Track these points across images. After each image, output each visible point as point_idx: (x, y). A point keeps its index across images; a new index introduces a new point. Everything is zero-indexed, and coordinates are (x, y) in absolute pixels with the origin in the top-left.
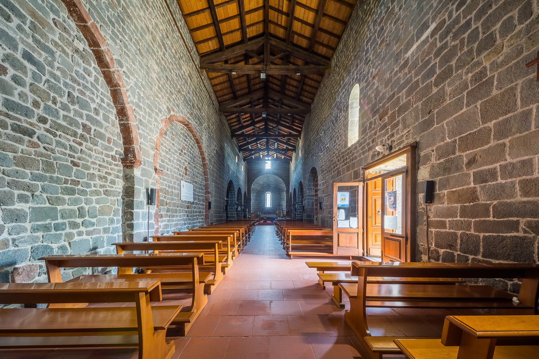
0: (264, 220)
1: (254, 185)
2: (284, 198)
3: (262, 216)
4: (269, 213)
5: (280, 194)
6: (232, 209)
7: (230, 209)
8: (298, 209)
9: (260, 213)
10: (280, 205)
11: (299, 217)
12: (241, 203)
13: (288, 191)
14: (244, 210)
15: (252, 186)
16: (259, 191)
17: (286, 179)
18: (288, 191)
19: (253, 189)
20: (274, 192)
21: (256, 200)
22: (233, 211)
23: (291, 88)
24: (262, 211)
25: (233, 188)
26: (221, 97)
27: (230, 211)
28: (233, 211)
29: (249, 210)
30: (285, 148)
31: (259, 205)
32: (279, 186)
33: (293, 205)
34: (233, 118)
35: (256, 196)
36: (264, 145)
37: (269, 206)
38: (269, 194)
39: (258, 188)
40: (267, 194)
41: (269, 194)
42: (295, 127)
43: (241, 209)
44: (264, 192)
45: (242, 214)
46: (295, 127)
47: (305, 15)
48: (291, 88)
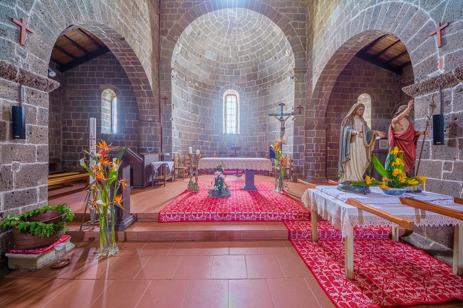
16: (205, 85)
17: (295, 25)
20: (248, 90)
37: (234, 131)
40: (229, 99)
41: (234, 99)
44: (218, 88)
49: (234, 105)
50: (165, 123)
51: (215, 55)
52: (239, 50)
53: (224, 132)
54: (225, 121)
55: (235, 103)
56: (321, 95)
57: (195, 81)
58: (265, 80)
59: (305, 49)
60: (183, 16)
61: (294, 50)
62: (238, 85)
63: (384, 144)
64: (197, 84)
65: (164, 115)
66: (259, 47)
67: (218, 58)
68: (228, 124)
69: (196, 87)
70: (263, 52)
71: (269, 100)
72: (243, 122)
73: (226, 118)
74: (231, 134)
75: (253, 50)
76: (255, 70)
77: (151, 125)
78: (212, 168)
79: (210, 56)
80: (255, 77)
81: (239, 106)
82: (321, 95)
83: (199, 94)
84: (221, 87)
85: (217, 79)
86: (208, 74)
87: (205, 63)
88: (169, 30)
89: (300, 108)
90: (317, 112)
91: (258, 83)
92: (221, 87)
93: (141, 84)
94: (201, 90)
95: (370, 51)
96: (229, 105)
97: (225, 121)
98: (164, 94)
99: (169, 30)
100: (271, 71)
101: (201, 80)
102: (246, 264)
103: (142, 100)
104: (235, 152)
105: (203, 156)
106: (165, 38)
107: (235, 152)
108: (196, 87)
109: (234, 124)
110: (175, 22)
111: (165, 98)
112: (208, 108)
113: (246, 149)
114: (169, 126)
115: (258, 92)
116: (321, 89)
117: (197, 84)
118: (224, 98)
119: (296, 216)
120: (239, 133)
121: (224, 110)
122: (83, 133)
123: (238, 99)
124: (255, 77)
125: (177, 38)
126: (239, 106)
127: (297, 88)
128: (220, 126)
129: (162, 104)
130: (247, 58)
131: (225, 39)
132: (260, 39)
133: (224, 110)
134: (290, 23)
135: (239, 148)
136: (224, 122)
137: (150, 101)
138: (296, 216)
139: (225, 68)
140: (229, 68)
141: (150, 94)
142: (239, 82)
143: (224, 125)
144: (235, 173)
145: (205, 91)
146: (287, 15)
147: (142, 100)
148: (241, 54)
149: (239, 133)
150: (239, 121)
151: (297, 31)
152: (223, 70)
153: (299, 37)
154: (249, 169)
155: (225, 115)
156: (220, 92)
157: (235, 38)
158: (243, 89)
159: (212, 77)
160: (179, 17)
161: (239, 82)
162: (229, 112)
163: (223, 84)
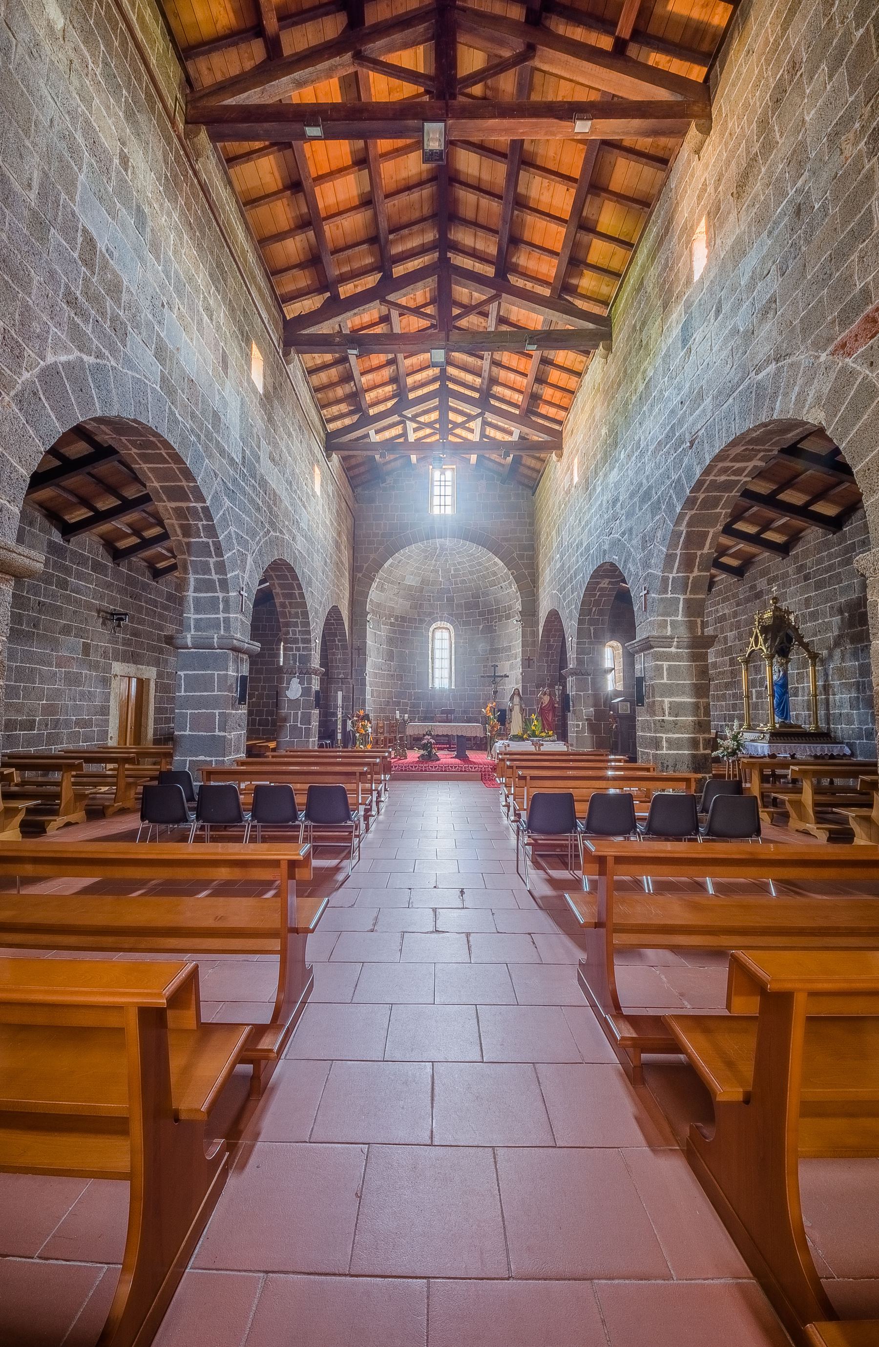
0: (424, 747)
1: (381, 588)
2: (509, 648)
3: (415, 728)
4: (448, 716)
5: (489, 630)
6: (206, 683)
7: (193, 683)
8: (669, 690)
9: (403, 712)
10: (495, 679)
11: (671, 744)
12: (305, 660)
13: (529, 613)
14: (323, 700)
15: (374, 594)
16: (403, 619)
17: (521, 557)
18: (529, 613)
19: (379, 605)
20: (466, 623)
21: (390, 656)
22: (215, 702)
23: (507, 393)
24: (414, 706)
25: (211, 531)
26: (330, 421)
27: (188, 702)
28: (215, 702)
29: (355, 700)
30: (515, 438)
31: (400, 678)
32: (486, 594)
33: (574, 673)
34: (338, 402)
35: (391, 641)
36: (430, 425)
37: (445, 684)
38: (446, 635)
39: (400, 605)
40: (438, 634)
41: (446, 635)
42: (540, 421)
43: (306, 692)
44: (421, 621)
45: (307, 720)
46: (540, 421)
47: (512, 376)
48: (507, 393)
49: (446, 644)
50: (357, 680)
51: (419, 579)
52: (452, 572)
53: (430, 686)
54: (433, 667)
55: (448, 651)
56: (550, 647)
57: (390, 616)
58: (490, 612)
59: (534, 587)
60: (382, 548)
61: (520, 588)
62: (451, 615)
63: (625, 708)
64: (392, 620)
65: (356, 670)
66: (479, 571)
67: (422, 582)
68: (437, 673)
69: (392, 624)
70: (484, 577)
71: (496, 641)
72: (461, 670)
73: (433, 663)
74: (442, 690)
75: (471, 573)
76: (476, 596)
77: (342, 683)
78: (421, 733)
79: (411, 581)
80: (476, 605)
81: (453, 646)
82: (550, 647)
83: (394, 632)
84: (426, 619)
85: (420, 608)
86: (408, 604)
87: (405, 590)
88: (365, 565)
89: (529, 659)
90: (549, 666)
91: (481, 614)
92: (426, 619)
93: (337, 637)
94: (399, 626)
95: (771, 487)
96: (437, 644)
97: (433, 667)
98: (357, 643)
99: (365, 565)
100: (497, 601)
101: (398, 613)
102: (478, 1020)
103: (334, 654)
104: (447, 717)
105: (412, 720)
106: (360, 575)
107: (447, 717)
108: (392, 624)
109: (446, 673)
110: (372, 556)
111: (359, 649)
112: (407, 651)
113: (465, 712)
114: (364, 684)
115: (481, 627)
116: (549, 641)
117: (392, 620)
118: (430, 634)
119: (491, 769)
120: (453, 687)
121: (430, 652)
122: (256, 693)
123: (453, 635)
124: (476, 605)
125: (375, 576)
126: (453, 646)
127: (524, 635)
128: (423, 677)
129: (355, 656)
130: (463, 582)
131: (433, 562)
132: (480, 564)
133: (430, 652)
134: (515, 555)
135: (451, 712)
136: (430, 671)
137: (344, 654)
138: (491, 769)
139: (433, 593)
140: (438, 592)
141: (345, 647)
142: (453, 611)
143: (430, 675)
144: (447, 748)
145: (403, 626)
146: (510, 545)
147: (334, 654)
148: (455, 576)
149: (453, 687)
150: (453, 668)
151: (523, 564)
152: (429, 596)
153: (526, 572)
154: (460, 734)
155: (433, 659)
156: (424, 625)
157: (447, 561)
158: (459, 622)
159: (414, 607)
160: (377, 549)
161: (453, 611)
162: (437, 654)
163: (431, 614)
